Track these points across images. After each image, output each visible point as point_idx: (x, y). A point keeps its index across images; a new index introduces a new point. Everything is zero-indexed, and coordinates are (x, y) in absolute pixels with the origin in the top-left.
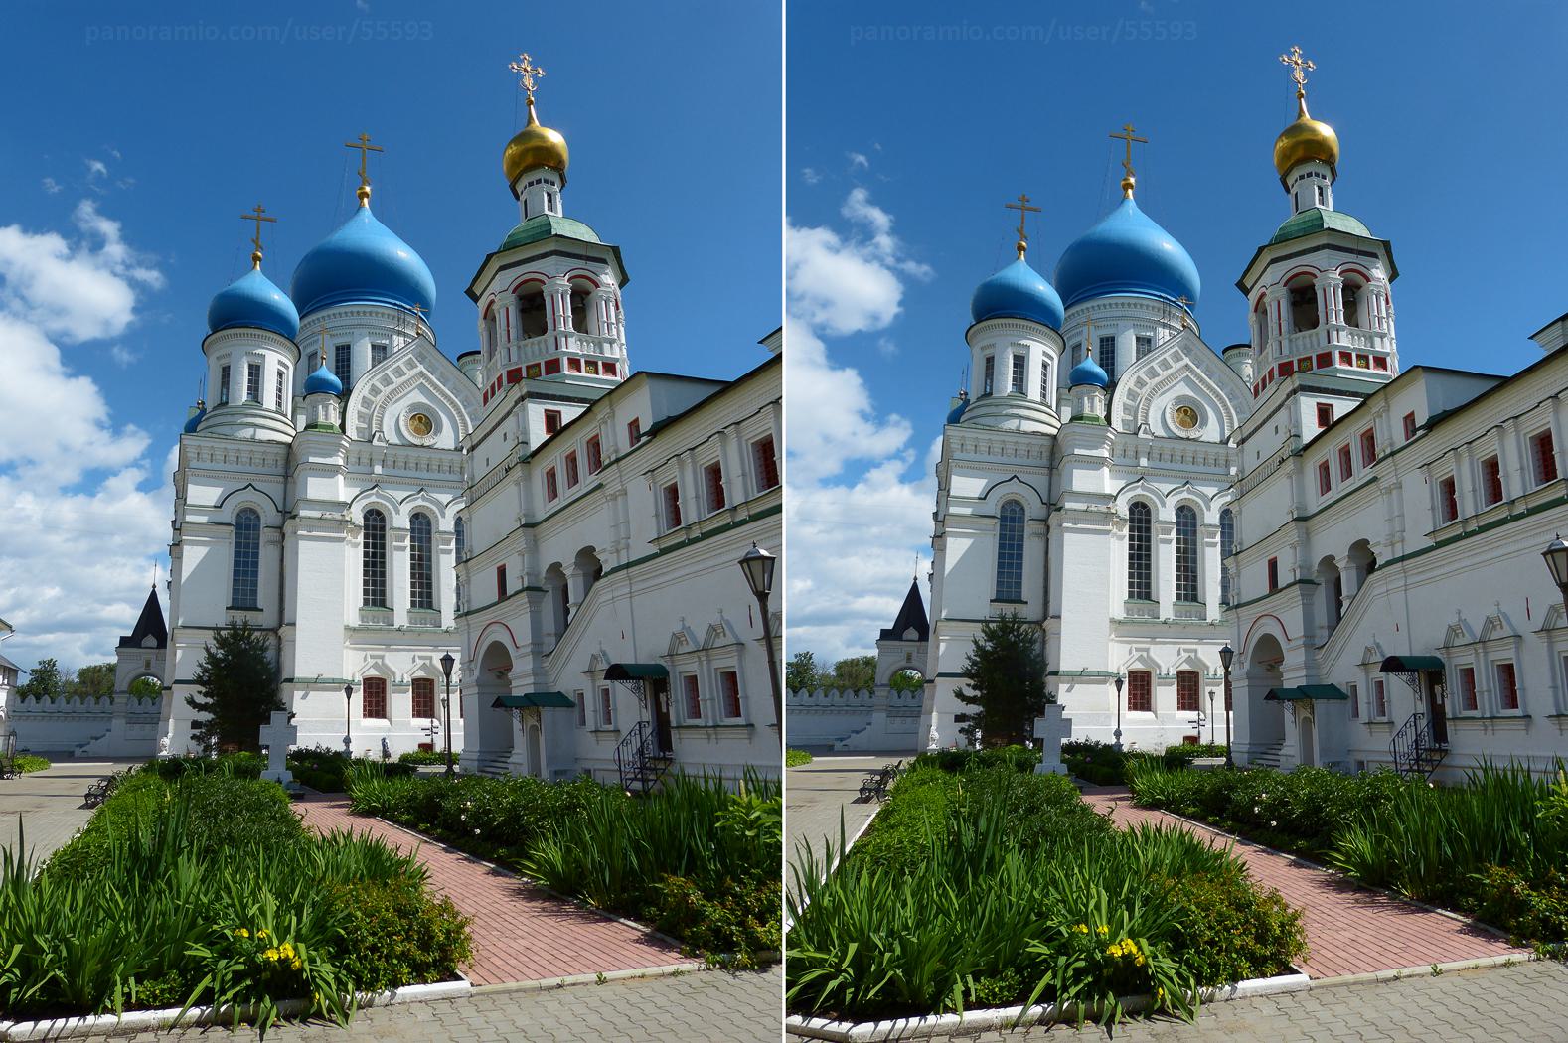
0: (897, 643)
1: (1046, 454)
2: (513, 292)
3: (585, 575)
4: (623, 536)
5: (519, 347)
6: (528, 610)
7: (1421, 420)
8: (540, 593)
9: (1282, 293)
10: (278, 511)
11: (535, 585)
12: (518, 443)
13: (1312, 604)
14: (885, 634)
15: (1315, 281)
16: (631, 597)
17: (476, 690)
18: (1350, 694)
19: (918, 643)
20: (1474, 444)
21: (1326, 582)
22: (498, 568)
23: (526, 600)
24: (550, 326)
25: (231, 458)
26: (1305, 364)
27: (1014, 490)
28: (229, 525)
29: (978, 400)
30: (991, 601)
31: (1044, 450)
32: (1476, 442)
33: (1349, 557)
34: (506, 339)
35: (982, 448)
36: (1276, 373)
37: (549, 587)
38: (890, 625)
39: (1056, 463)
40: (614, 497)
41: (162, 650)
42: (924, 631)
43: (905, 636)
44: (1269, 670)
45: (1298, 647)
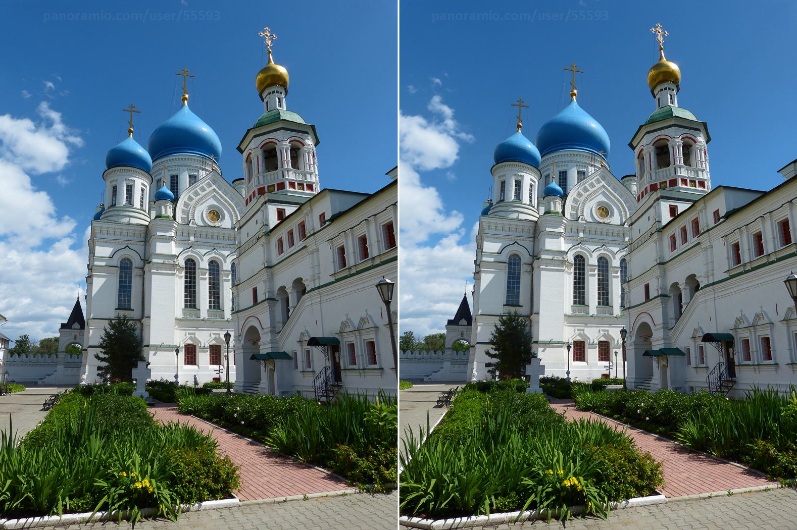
0: (456, 327)
1: (532, 231)
2: (261, 148)
3: (297, 292)
4: (317, 273)
5: (656, 173)
6: (268, 310)
8: (274, 302)
9: (652, 149)
10: (141, 260)
11: (272, 297)
12: (264, 225)
13: (667, 307)
14: (450, 322)
15: (668, 143)
16: (321, 303)
17: (242, 351)
18: (686, 353)
19: (467, 327)
20: (749, 226)
21: (674, 296)
22: (253, 289)
23: (267, 305)
24: (280, 166)
25: (118, 233)
26: (663, 185)
28: (116, 267)
30: (504, 305)
31: (530, 229)
32: (750, 225)
33: (686, 283)
34: (257, 172)
35: (499, 228)
36: (649, 189)
37: (279, 298)
38: (452, 318)
39: (537, 235)
41: (82, 330)
42: (470, 321)
43: (460, 323)
44: (645, 341)
45: (660, 329)
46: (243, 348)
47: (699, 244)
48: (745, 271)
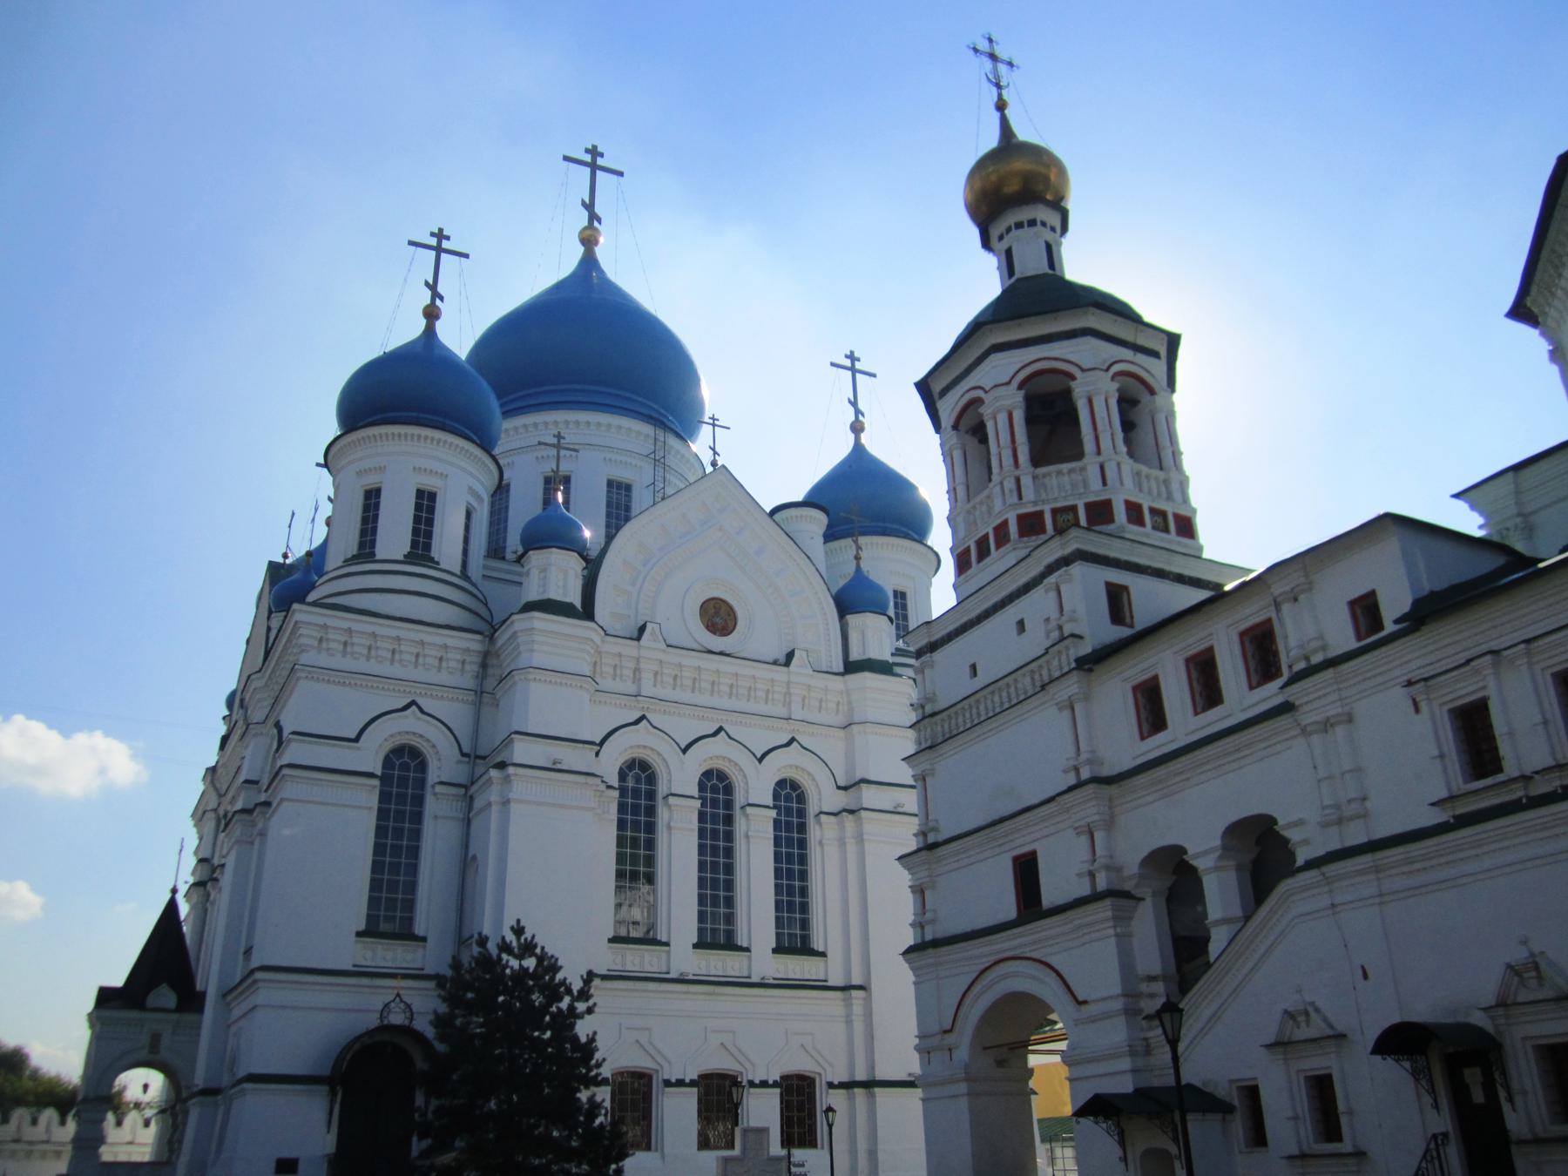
0: (134, 1014)
1: (472, 668)
2: (1020, 387)
3: (1239, 868)
4: (1353, 795)
5: (1035, 477)
6: (1111, 931)
7: (1394, 605)
8: (1131, 903)
9: (1014, 399)
11: (1118, 887)
12: (1062, 639)
13: (1130, 935)
14: (106, 997)
16: (1381, 903)
17: (963, 1088)
18: (1236, 1102)
19: (175, 1016)
20: (1535, 644)
21: (1154, 895)
22: (1016, 860)
23: (1109, 913)
24: (1089, 446)
25: (429, 660)
26: (1065, 518)
27: (408, 727)
28: (370, 775)
29: (349, 562)
30: (359, 934)
31: (468, 659)
32: (1541, 642)
33: (1225, 848)
34: (1011, 461)
35: (406, 657)
36: (1013, 528)
37: (1145, 891)
38: (118, 979)
39: (490, 684)
40: (1327, 725)
41: (190, 1017)
42: (191, 1000)
43: (151, 1001)
44: (1001, 1063)
45: (1107, 1016)
46: (968, 1079)
47: (1286, 708)
48: (1528, 798)
